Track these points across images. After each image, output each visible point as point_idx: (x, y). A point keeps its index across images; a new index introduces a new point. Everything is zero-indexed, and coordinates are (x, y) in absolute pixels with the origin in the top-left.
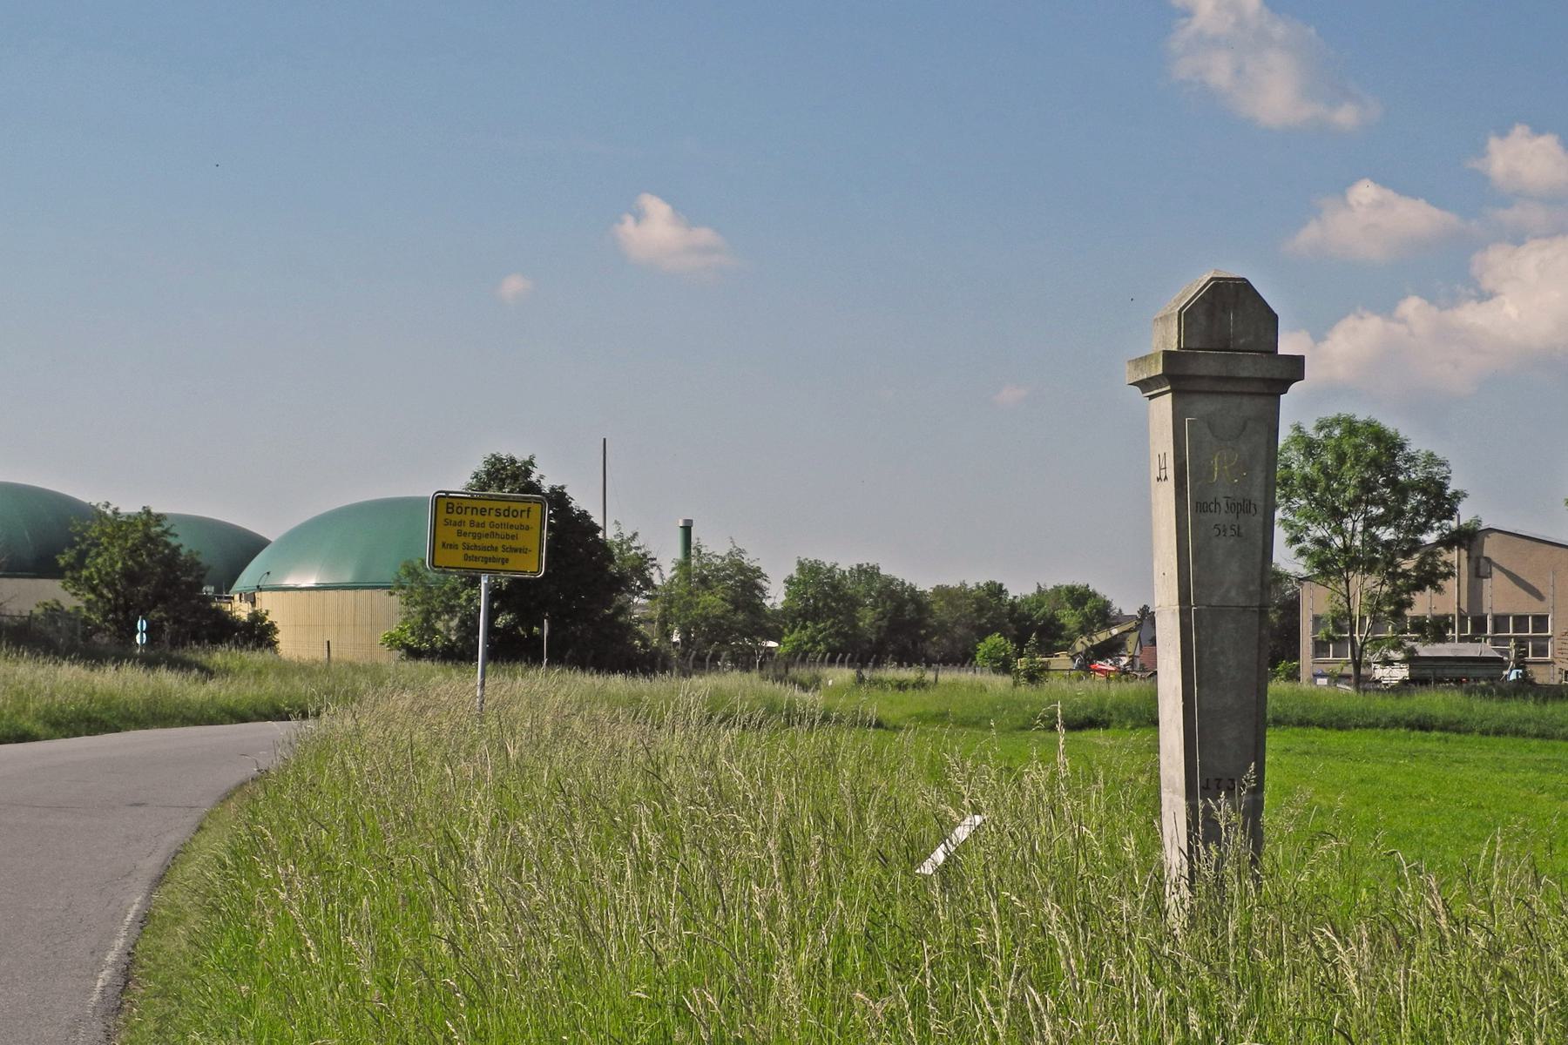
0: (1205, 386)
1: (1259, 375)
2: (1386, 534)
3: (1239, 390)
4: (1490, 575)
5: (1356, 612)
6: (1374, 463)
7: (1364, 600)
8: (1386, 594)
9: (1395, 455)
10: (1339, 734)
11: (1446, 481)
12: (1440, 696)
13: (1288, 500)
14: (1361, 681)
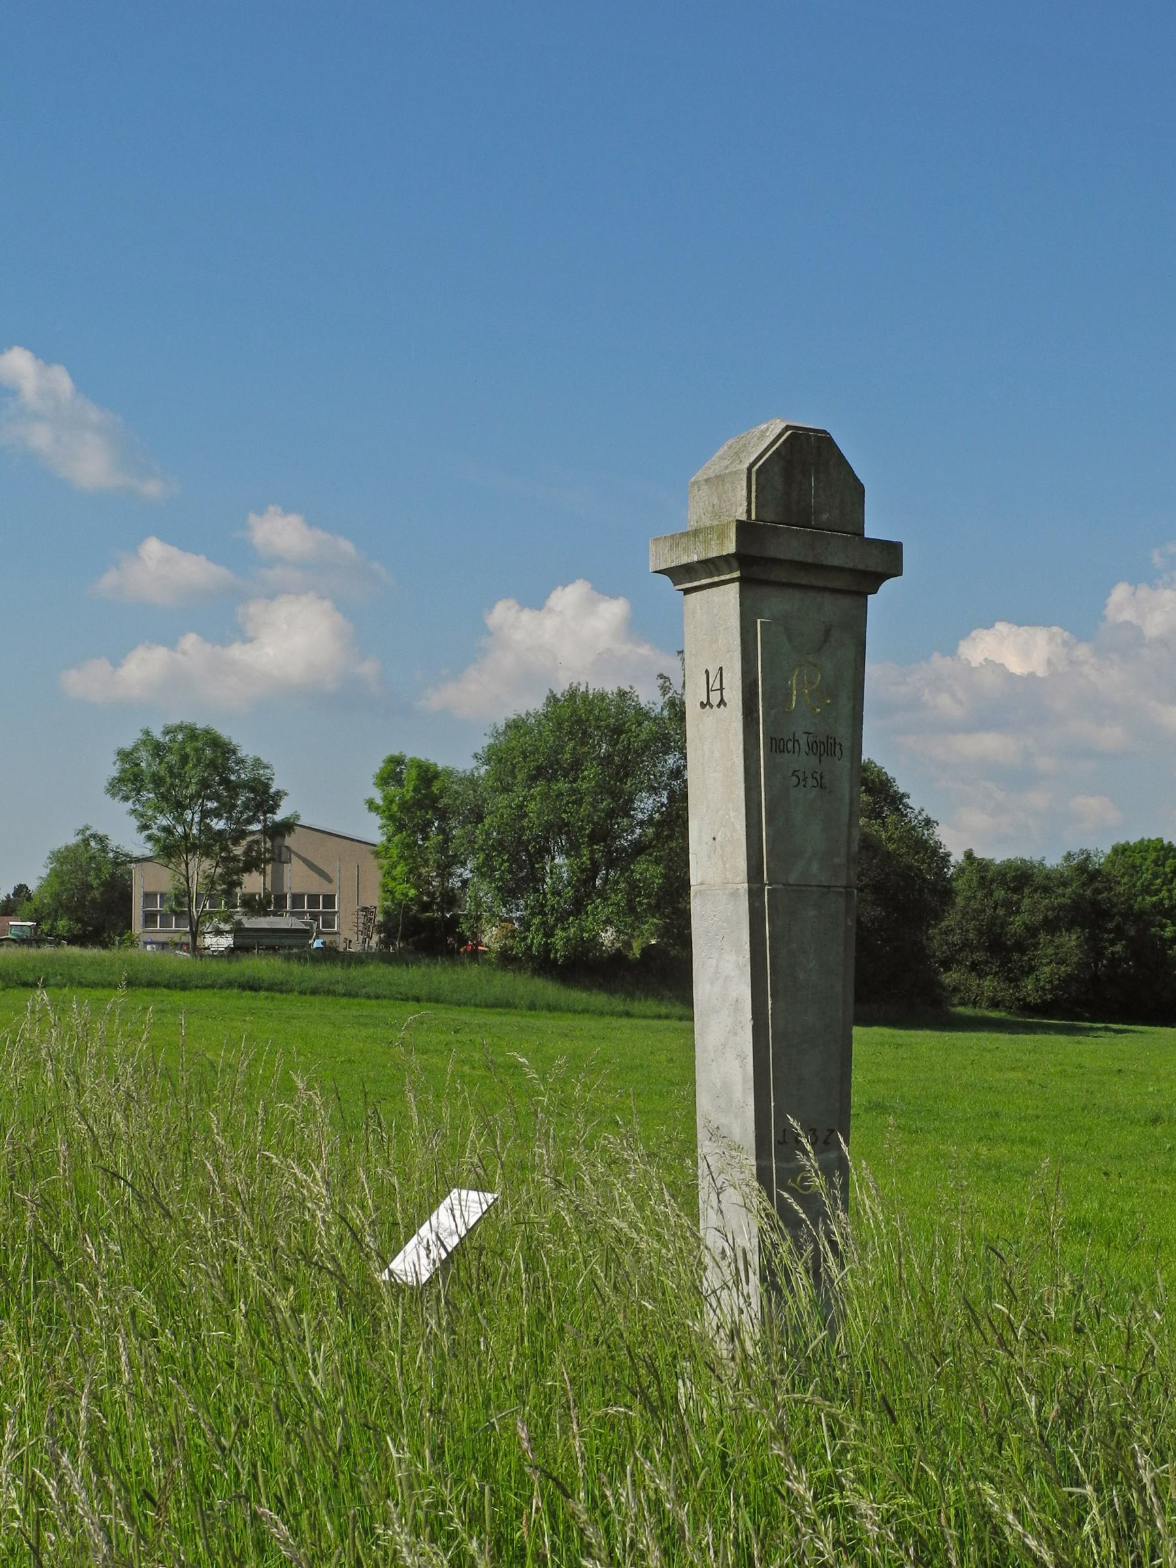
0: (781, 575)
1: (850, 565)
2: (218, 825)
3: (821, 583)
4: (289, 861)
5: (194, 890)
6: (212, 764)
7: (201, 880)
8: (221, 875)
9: (228, 759)
10: (183, 994)
11: (270, 782)
12: (264, 962)
13: (138, 792)
14: (196, 950)
